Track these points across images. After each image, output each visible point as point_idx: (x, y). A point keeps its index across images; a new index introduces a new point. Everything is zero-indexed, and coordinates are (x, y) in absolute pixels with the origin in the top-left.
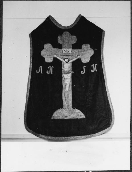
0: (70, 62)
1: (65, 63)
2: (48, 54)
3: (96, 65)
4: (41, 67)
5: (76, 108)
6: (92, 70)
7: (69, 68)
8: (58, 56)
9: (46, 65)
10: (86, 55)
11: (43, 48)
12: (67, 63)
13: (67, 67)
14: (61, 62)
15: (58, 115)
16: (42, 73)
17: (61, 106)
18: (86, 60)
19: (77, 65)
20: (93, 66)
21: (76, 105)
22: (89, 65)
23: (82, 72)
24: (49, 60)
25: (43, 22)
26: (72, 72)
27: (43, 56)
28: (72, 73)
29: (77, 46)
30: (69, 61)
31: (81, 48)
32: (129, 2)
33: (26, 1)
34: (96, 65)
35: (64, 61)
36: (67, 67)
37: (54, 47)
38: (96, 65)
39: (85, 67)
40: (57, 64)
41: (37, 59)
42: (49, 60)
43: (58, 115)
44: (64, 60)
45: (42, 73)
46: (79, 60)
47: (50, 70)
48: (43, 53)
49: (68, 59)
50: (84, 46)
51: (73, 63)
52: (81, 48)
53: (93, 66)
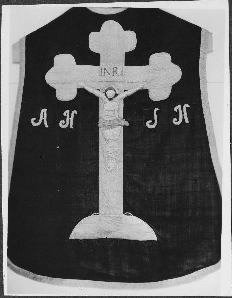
0: (118, 97)
1: (107, 100)
2: (65, 76)
3: (187, 108)
4: (44, 111)
5: (134, 214)
6: (175, 119)
7: (116, 113)
8: (87, 86)
9: (58, 109)
10: (160, 75)
11: (51, 65)
12: (110, 99)
13: (111, 113)
14: (96, 99)
15: (85, 229)
16: (47, 126)
17: (94, 208)
18: (160, 93)
19: (138, 104)
20: (178, 110)
21: (129, 207)
22: (167, 107)
23: (151, 124)
24: (65, 94)
25: (50, 23)
26: (126, 123)
27: (52, 86)
28: (125, 127)
29: (137, 58)
30: (116, 95)
31: (146, 62)
32: (3, 7)
33: (231, 244)
34: (187, 108)
35: (103, 96)
36: (111, 113)
37: (79, 62)
38: (186, 106)
39: (158, 111)
40: (86, 103)
41: (36, 92)
42: (65, 94)
43: (85, 229)
44: (105, 94)
45: (47, 126)
46: (143, 94)
47: (68, 120)
48: (51, 77)
49: (113, 92)
50: (154, 58)
51: (128, 101)
52: (146, 62)
53: (178, 110)
